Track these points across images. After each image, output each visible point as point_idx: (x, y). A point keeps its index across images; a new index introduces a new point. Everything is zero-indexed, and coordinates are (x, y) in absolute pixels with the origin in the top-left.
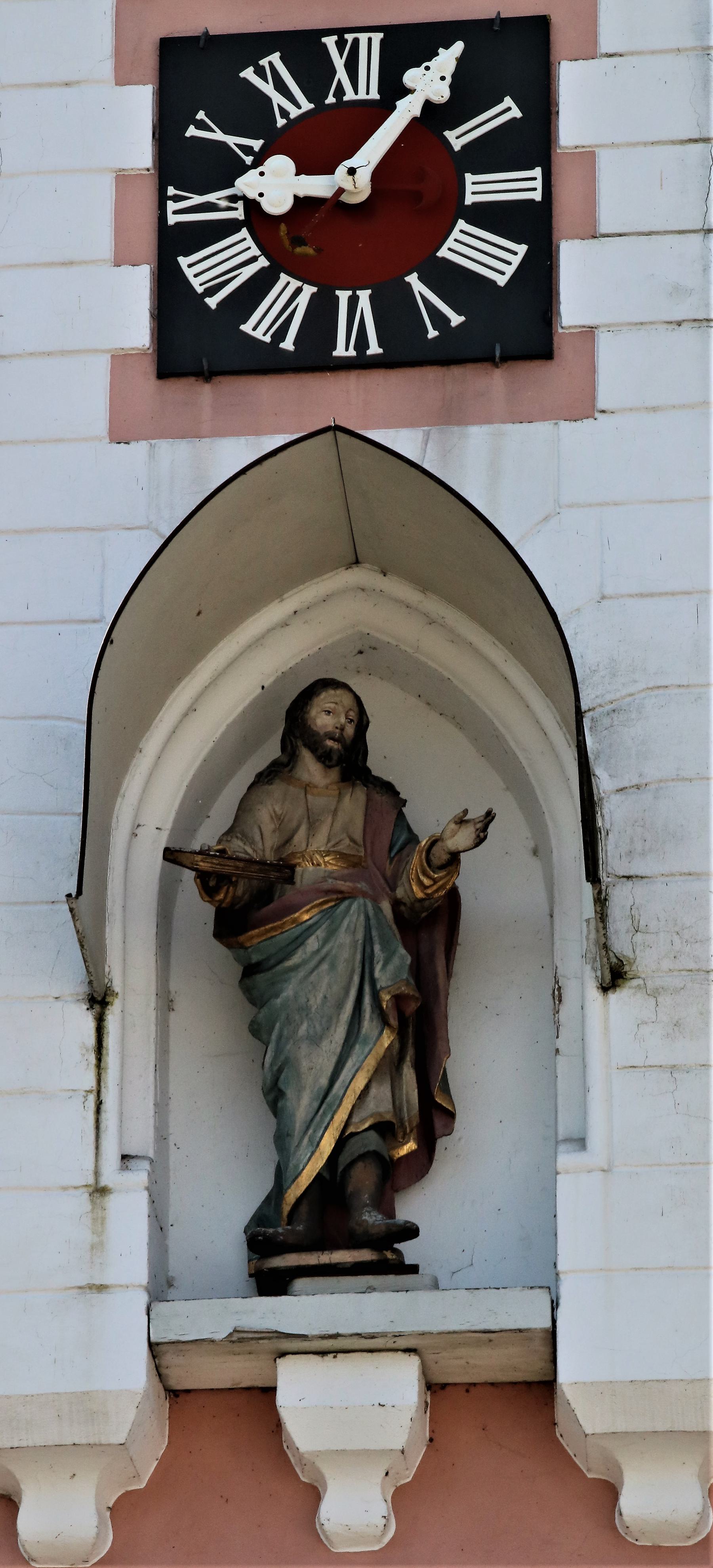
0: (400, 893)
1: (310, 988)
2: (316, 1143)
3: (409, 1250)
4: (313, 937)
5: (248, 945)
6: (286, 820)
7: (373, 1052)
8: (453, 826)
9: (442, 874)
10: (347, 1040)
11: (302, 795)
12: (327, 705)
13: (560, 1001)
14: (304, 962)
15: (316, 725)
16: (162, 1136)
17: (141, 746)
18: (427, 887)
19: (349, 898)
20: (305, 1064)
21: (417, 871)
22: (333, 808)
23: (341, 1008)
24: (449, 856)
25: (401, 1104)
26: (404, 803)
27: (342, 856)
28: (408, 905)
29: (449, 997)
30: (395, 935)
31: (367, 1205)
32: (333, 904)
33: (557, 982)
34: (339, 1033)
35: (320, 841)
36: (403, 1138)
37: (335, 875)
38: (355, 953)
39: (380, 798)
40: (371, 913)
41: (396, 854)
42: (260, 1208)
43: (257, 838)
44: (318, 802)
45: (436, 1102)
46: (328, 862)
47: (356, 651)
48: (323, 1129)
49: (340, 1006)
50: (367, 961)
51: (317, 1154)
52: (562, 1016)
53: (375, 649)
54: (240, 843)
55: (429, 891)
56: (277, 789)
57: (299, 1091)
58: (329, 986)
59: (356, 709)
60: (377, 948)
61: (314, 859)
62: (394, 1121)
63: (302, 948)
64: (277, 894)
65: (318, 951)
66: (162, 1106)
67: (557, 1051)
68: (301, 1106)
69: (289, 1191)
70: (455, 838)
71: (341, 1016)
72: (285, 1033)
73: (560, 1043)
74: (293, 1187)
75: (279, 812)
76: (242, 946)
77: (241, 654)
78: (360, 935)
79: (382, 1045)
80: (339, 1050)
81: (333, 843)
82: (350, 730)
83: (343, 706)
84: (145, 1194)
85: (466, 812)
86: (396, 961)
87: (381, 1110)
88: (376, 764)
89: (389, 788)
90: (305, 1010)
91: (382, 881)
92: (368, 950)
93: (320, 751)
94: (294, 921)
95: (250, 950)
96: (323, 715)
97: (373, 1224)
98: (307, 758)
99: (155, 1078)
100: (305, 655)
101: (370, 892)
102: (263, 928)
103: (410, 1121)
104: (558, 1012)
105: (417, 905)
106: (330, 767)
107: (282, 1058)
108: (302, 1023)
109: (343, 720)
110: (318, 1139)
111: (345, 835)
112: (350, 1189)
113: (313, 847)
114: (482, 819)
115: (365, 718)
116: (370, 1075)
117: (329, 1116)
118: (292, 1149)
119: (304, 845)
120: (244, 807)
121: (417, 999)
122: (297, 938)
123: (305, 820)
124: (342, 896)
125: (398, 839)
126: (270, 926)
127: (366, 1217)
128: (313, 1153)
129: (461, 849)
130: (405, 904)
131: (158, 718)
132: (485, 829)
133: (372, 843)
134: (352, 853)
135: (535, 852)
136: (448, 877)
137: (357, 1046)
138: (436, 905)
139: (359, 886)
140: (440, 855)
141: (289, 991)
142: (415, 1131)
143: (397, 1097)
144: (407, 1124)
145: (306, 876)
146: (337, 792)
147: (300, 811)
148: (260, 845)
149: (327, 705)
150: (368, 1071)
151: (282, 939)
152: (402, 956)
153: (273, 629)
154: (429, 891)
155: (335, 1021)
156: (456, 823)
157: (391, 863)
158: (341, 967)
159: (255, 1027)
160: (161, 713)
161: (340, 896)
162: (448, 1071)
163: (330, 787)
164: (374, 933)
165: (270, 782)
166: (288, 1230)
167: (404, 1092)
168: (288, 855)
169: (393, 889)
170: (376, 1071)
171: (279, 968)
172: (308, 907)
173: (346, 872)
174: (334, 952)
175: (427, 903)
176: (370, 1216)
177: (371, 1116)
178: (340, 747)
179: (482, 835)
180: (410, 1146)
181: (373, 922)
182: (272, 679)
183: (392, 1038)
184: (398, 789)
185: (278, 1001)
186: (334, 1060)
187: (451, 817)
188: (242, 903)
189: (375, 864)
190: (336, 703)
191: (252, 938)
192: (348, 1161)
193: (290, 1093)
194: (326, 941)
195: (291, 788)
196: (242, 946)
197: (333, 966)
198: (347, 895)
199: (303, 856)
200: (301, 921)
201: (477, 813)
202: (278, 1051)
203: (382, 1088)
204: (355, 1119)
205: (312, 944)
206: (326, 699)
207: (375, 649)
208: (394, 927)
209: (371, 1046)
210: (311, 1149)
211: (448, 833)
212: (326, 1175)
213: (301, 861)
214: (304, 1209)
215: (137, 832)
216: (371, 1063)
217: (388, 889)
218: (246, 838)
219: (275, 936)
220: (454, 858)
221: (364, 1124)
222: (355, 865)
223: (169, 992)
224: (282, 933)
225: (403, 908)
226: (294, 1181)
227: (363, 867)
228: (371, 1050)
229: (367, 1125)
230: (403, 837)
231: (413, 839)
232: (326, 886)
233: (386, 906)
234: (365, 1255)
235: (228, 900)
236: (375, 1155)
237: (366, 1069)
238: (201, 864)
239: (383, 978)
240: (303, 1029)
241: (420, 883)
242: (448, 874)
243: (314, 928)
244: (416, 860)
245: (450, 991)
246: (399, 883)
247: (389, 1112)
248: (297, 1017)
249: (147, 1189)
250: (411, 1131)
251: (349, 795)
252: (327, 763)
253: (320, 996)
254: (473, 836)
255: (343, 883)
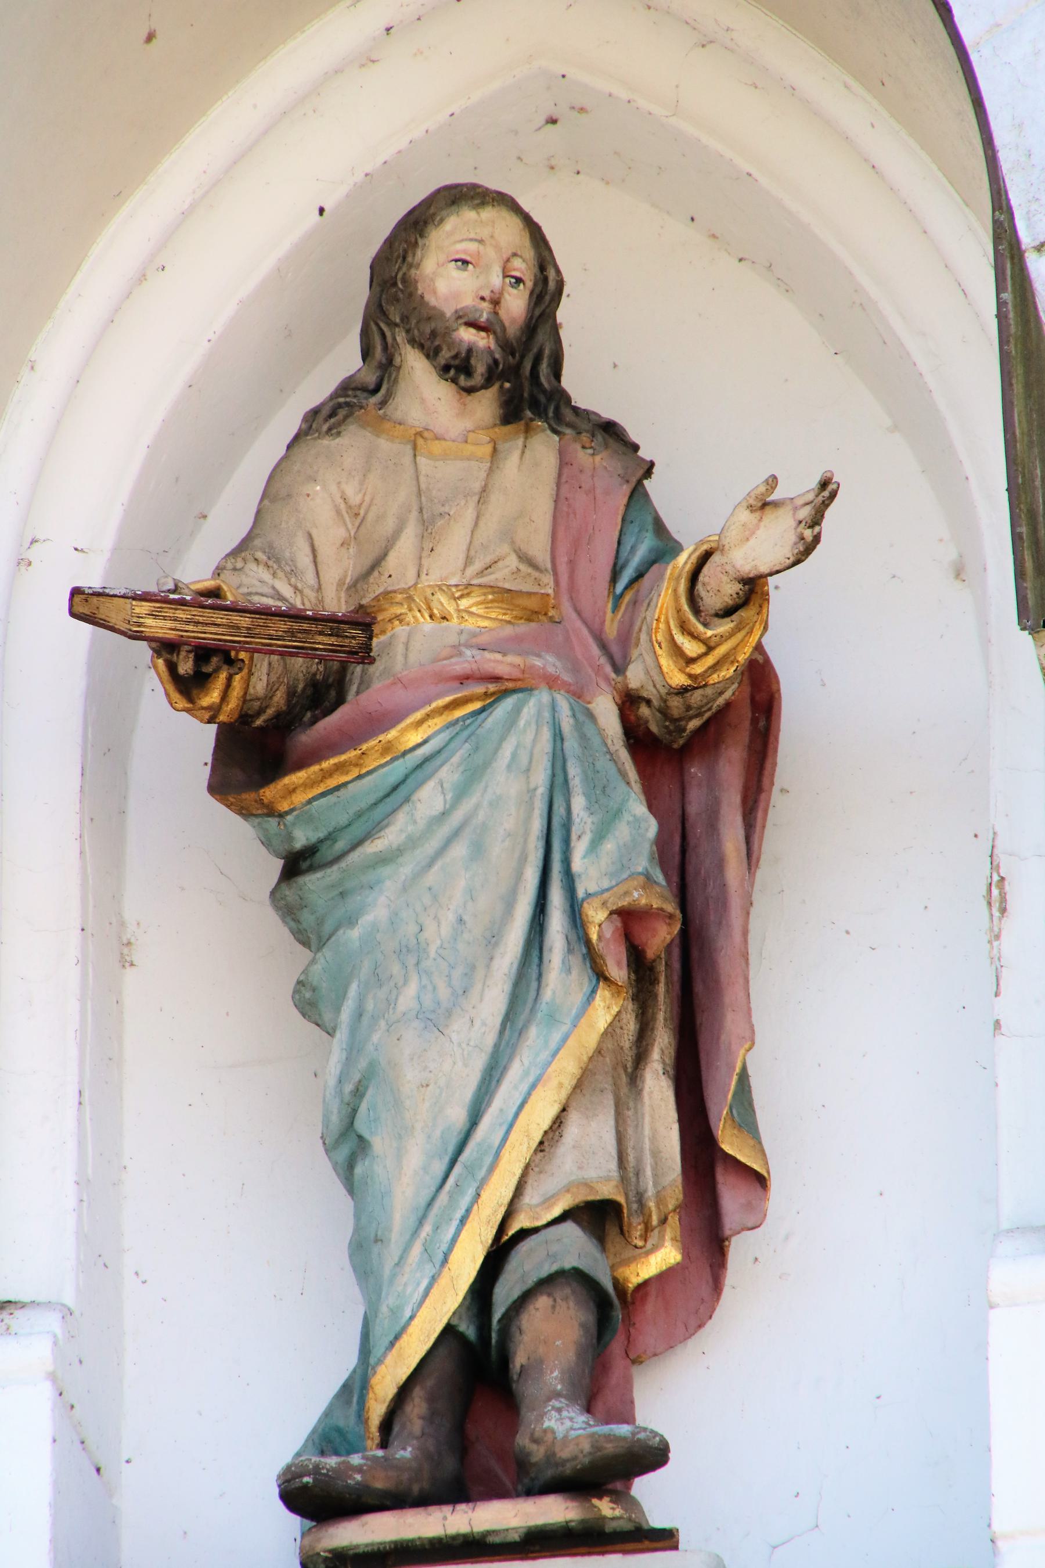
0: (635, 677)
1: (427, 899)
2: (440, 1257)
3: (654, 1497)
4: (431, 784)
5: (284, 806)
6: (371, 516)
7: (571, 1042)
8: (745, 516)
9: (725, 627)
10: (509, 1017)
11: (407, 460)
12: (459, 246)
13: (1003, 910)
14: (413, 842)
15: (435, 292)
16: (99, 1255)
17: (32, 356)
18: (691, 661)
19: (514, 691)
20: (410, 1076)
21: (668, 623)
22: (477, 486)
23: (496, 944)
24: (737, 587)
25: (639, 1160)
26: (649, 469)
27: (503, 595)
28: (656, 703)
29: (753, 911)
30: (623, 774)
31: (558, 1395)
32: (477, 705)
33: (995, 866)
34: (492, 1000)
35: (447, 563)
36: (645, 1238)
37: (483, 639)
38: (528, 819)
39: (596, 462)
40: (567, 724)
41: (626, 588)
42: (327, 1414)
43: (304, 560)
44: (441, 472)
45: (722, 1150)
46: (466, 611)
47: (542, 120)
48: (455, 1223)
49: (493, 939)
50: (555, 838)
51: (443, 1281)
52: (1007, 945)
53: (582, 110)
54: (266, 576)
55: (697, 669)
56: (352, 443)
57: (400, 1137)
58: (471, 895)
59: (529, 253)
60: (578, 803)
61: (435, 605)
62: (621, 1199)
63: (406, 808)
64: (354, 688)
65: (444, 814)
66: (98, 1186)
67: (997, 1024)
68: (404, 1168)
69: (382, 1370)
70: (752, 542)
71: (496, 963)
72: (370, 1006)
73: (1004, 1008)
74: (389, 1359)
75: (355, 499)
76: (271, 811)
77: (266, 132)
78: (541, 778)
79: (592, 1026)
80: (490, 1039)
81: (478, 566)
82: (516, 305)
83: (497, 248)
84: (46, 1390)
85: (773, 482)
86: (622, 831)
87: (591, 1174)
88: (584, 383)
89: (610, 431)
90: (412, 952)
91: (595, 650)
92: (559, 810)
93: (445, 355)
94: (387, 748)
95: (289, 818)
96: (453, 270)
97: (565, 1437)
98: (417, 370)
99: (80, 1122)
100: (418, 133)
101: (567, 677)
102: (315, 768)
103: (660, 1200)
104: (998, 937)
105: (675, 703)
106: (470, 391)
107: (362, 1064)
108: (406, 982)
109: (496, 279)
110: (444, 1247)
111: (506, 548)
112: (519, 1359)
113: (431, 579)
114: (810, 496)
115: (551, 274)
116: (564, 1094)
117: (471, 1192)
118: (387, 1272)
119: (411, 573)
120: (275, 492)
121: (671, 916)
122: (395, 788)
123: (414, 514)
124: (499, 688)
125: (633, 549)
126: (333, 761)
127: (551, 1422)
128: (434, 1279)
129: (764, 569)
130: (648, 702)
131: (71, 289)
132: (816, 520)
133: (572, 563)
134: (526, 588)
135: (959, 572)
136: (740, 636)
137: (533, 1031)
138: (721, 701)
139: (538, 663)
140: (719, 587)
141: (377, 910)
142: (674, 1220)
143: (630, 1144)
144: (652, 1204)
145: (416, 645)
146: (489, 448)
147: (404, 493)
148: (310, 578)
149: (459, 246)
150: (561, 1085)
151: (363, 791)
152: (638, 822)
153: (338, 71)
154: (697, 669)
155: (480, 972)
156: (750, 507)
157: (616, 608)
158: (498, 849)
159: (308, 995)
160: (79, 276)
161: (492, 687)
162: (754, 1082)
163: (471, 437)
164: (574, 770)
165: (334, 431)
166: (375, 1458)
167: (647, 1131)
168: (376, 599)
169: (619, 669)
170: (578, 1086)
171: (355, 857)
172: (418, 715)
173: (509, 630)
174: (481, 815)
175: (696, 698)
176: (561, 1420)
177: (567, 1190)
178: (493, 345)
179: (808, 534)
180: (664, 1256)
181: (571, 745)
182: (342, 191)
183: (615, 1009)
184: (634, 436)
185: (354, 935)
186: (479, 1063)
187: (740, 496)
188: (270, 712)
189: (579, 613)
190: (481, 241)
191: (292, 791)
192: (516, 1294)
193: (379, 1143)
194: (461, 792)
195: (384, 444)
196: (271, 811)
197: (478, 850)
198: (510, 685)
199: (410, 599)
200: (403, 748)
201: (798, 485)
202: (353, 1050)
203: (593, 1124)
204: (530, 1198)
205: (429, 799)
206: (456, 232)
207: (582, 110)
208: (624, 755)
209: (564, 1029)
210: (429, 1270)
211: (732, 536)
212: (468, 1329)
213: (403, 610)
214: (417, 1408)
215: (32, 554)
216: (566, 1069)
217: (608, 669)
218: (275, 560)
219: (345, 784)
220: (752, 590)
221: (550, 1207)
222: (531, 616)
223: (122, 924)
224: (360, 777)
225: (644, 711)
226: (392, 1344)
227: (551, 620)
228: (565, 1039)
229: (556, 1212)
230: (644, 546)
231: (666, 546)
232: (459, 666)
233: (606, 710)
234: (554, 1511)
235: (233, 702)
236: (580, 1278)
237: (554, 1083)
238: (149, 621)
239: (593, 872)
240: (407, 999)
241: (677, 651)
242: (738, 629)
243: (437, 761)
244: (666, 595)
245: (756, 897)
246: (635, 653)
247: (608, 1179)
248: (396, 969)
249: (53, 1377)
250: (664, 1221)
251: (516, 454)
252: (462, 380)
253: (449, 918)
254: (792, 538)
255: (498, 656)
